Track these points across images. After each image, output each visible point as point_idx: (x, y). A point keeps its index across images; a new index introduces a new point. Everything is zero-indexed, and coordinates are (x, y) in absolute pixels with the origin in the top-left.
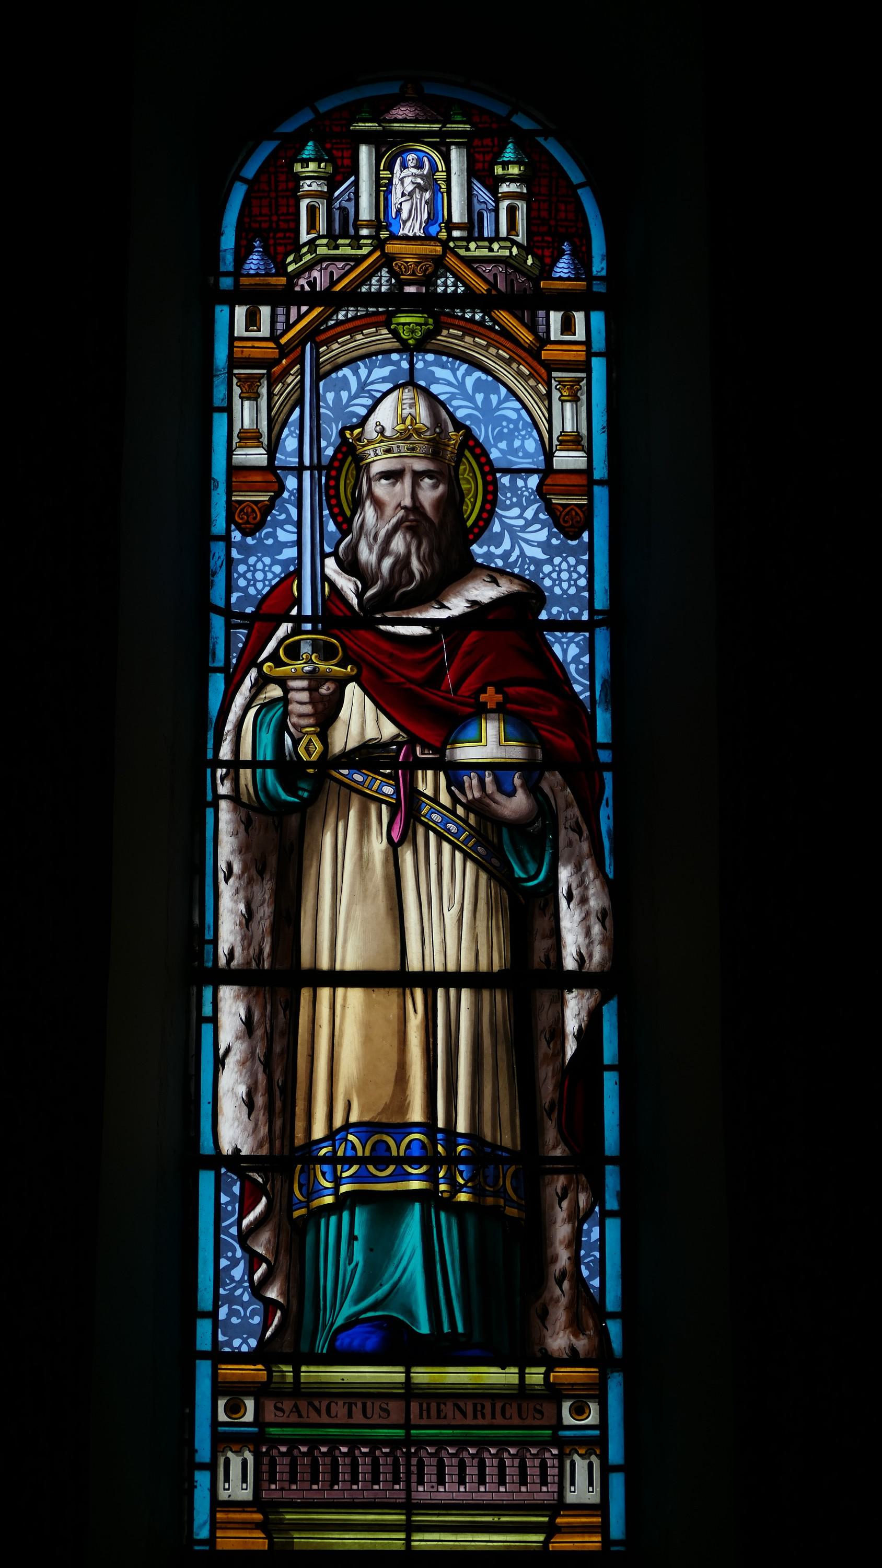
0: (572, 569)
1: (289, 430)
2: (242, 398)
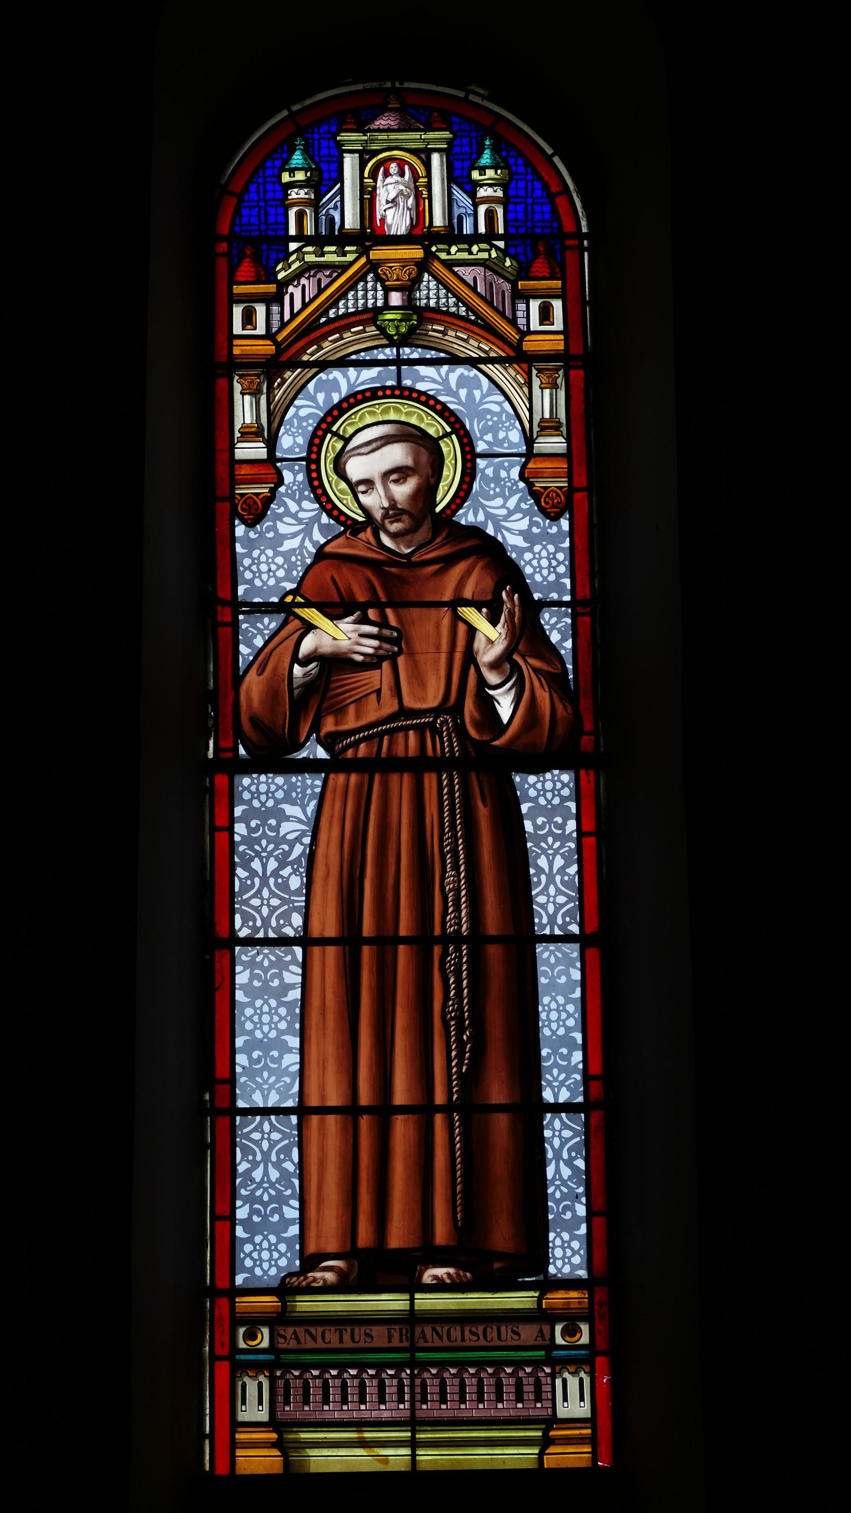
0: (551, 557)
1: (285, 428)
2: (243, 394)
